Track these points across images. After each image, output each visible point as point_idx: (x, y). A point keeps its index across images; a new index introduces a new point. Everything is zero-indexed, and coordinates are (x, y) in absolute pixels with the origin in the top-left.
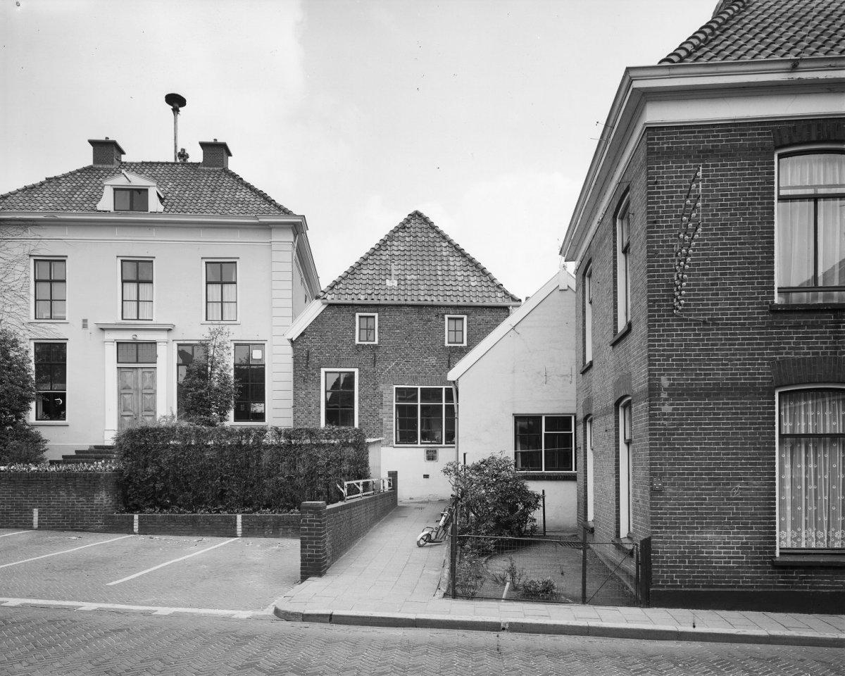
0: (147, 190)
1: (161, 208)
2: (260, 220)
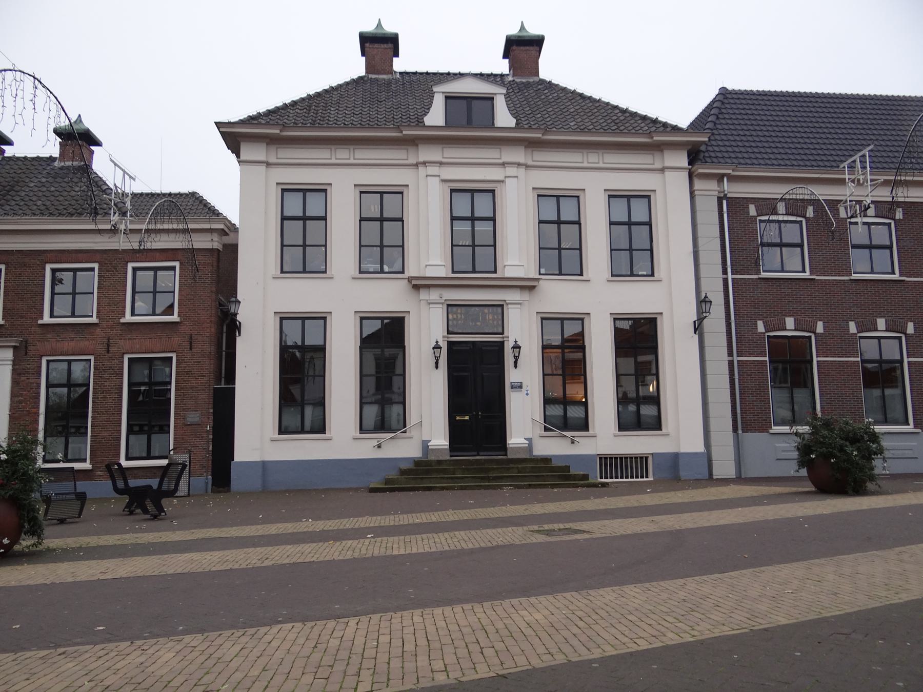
0: (492, 99)
1: (511, 122)
2: (655, 138)
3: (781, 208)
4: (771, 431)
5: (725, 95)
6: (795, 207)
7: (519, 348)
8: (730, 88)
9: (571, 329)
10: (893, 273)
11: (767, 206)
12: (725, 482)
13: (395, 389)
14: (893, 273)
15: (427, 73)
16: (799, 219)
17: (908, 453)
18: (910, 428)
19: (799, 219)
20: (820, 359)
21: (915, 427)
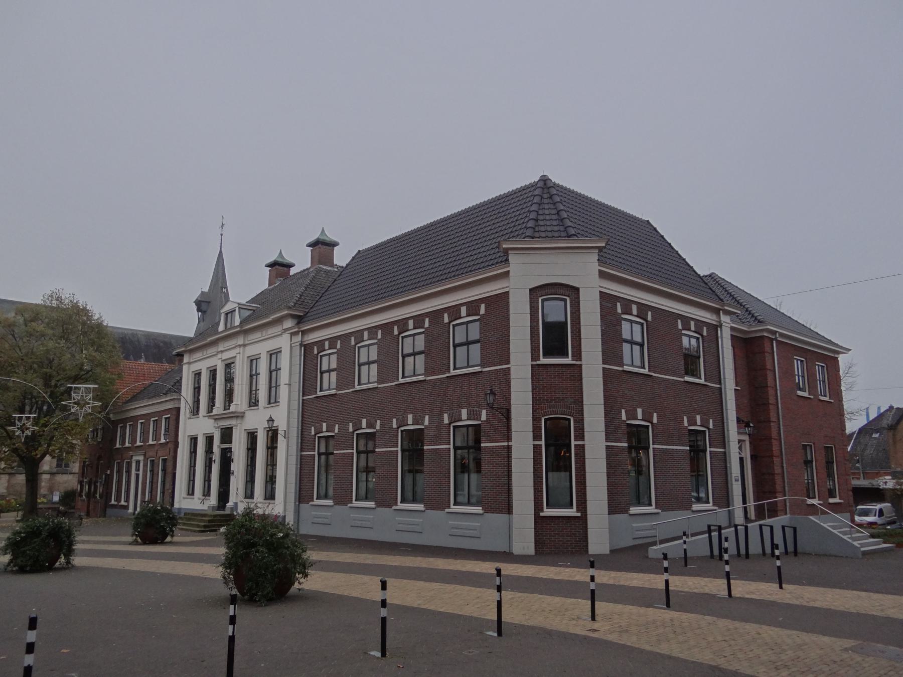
6: (643, 309)
8: (556, 179)
11: (627, 304)
13: (779, 488)
18: (651, 509)
21: (714, 505)
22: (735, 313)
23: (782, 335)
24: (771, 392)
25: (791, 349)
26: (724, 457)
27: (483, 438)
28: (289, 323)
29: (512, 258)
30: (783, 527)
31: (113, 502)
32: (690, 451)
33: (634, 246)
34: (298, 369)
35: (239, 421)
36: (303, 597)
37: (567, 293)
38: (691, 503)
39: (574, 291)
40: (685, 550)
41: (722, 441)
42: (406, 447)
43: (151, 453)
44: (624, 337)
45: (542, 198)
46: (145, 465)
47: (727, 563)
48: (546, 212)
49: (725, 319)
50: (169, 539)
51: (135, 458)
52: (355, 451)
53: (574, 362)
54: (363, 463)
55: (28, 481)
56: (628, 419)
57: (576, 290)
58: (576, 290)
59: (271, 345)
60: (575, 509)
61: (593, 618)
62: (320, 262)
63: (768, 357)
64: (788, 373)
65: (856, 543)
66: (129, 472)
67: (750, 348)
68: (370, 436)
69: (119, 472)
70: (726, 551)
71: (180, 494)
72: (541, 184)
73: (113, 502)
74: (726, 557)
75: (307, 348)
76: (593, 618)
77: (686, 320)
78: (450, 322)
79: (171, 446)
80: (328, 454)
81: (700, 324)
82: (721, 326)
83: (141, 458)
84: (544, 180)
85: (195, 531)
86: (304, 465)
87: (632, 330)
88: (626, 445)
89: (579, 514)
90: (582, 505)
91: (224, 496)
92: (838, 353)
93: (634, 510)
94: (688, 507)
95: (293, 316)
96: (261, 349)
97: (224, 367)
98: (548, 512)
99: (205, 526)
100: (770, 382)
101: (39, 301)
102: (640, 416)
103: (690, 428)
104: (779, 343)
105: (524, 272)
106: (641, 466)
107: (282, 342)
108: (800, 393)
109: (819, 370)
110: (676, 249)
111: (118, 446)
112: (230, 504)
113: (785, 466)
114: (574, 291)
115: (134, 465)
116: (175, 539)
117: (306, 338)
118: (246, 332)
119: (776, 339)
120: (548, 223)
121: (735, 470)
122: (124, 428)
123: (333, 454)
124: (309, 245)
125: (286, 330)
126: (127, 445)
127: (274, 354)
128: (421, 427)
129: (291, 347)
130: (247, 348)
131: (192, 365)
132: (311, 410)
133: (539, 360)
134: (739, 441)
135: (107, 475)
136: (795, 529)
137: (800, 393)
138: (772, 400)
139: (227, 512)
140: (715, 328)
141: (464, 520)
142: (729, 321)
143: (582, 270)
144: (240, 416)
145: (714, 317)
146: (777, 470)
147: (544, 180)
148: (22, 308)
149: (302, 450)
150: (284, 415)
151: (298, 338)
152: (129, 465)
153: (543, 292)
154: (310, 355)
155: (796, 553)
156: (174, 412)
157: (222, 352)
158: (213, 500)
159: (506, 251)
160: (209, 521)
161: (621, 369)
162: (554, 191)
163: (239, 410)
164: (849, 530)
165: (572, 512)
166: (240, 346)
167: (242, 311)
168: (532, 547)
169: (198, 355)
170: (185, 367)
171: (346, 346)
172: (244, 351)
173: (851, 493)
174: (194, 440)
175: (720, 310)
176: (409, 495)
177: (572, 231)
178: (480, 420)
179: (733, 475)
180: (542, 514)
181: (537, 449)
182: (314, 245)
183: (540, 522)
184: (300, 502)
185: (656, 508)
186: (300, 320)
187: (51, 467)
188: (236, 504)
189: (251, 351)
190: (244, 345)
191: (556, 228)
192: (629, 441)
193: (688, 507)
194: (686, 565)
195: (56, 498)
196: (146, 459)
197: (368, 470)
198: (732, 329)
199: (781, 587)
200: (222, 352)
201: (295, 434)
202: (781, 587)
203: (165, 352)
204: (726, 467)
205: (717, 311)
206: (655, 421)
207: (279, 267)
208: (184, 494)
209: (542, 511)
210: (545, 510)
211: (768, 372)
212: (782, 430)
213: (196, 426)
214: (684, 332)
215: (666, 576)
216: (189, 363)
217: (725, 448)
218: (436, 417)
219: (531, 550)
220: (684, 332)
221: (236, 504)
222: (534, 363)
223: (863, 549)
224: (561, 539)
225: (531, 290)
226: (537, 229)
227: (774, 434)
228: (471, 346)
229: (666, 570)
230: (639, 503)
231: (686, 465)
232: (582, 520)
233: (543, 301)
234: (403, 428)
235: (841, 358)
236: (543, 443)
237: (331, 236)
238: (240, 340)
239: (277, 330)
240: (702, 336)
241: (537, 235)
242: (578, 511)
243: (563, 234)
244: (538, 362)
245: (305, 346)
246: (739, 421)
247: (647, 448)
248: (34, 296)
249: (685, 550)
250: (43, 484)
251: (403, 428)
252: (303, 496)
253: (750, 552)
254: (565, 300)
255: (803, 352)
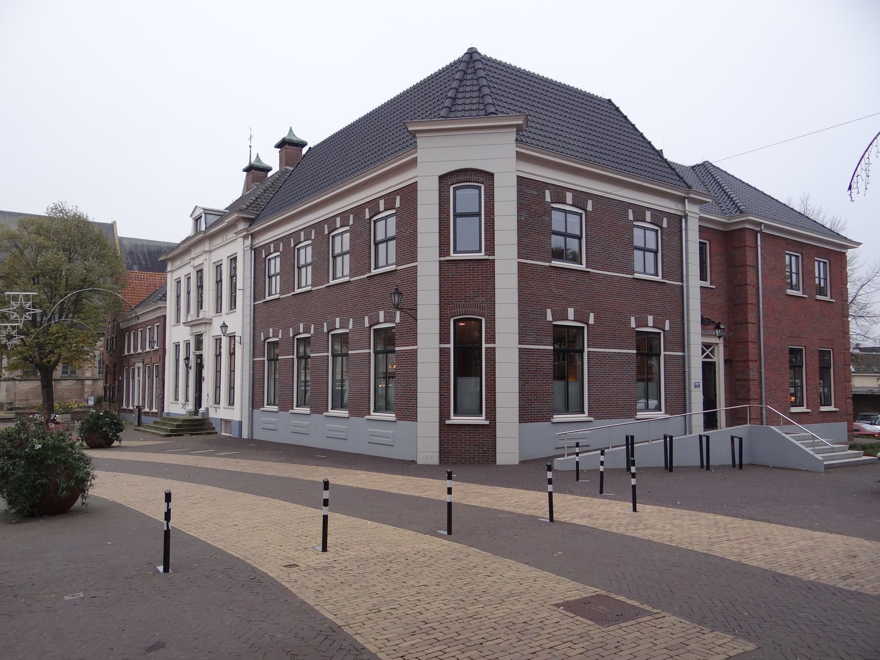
3: (569, 197)
4: (554, 420)
5: (472, 58)
6: (580, 198)
7: (791, 367)
8: (483, 51)
9: (199, 268)
10: (657, 275)
11: (559, 193)
12: (687, 469)
13: (753, 395)
14: (657, 275)
15: (617, 109)
16: (656, 228)
17: (304, 430)
18: (584, 417)
19: (656, 228)
20: (591, 349)
21: (589, 416)
22: (707, 202)
23: (767, 226)
24: (751, 290)
25: (780, 243)
26: (683, 362)
27: (397, 342)
28: (242, 226)
29: (421, 141)
30: (732, 438)
31: (124, 407)
32: (637, 354)
33: (589, 127)
34: (250, 274)
35: (208, 327)
36: (72, 511)
37: (481, 179)
38: (636, 411)
39: (488, 177)
40: (577, 462)
41: (680, 341)
42: (577, 356)
43: (147, 361)
44: (554, 228)
45: (465, 73)
46: (144, 372)
47: (634, 476)
48: (472, 88)
49: (689, 207)
50: (116, 443)
51: (137, 365)
52: (295, 357)
53: (486, 257)
54: (382, 369)
55: (43, 387)
56: (637, 326)
57: (491, 175)
58: (491, 175)
59: (228, 251)
60: (484, 417)
61: (325, 549)
62: (287, 165)
63: (749, 253)
64: (776, 269)
65: (819, 457)
66: (133, 378)
67: (729, 245)
68: (306, 341)
69: (128, 379)
70: (633, 464)
71: (168, 398)
72: (467, 58)
73: (124, 407)
74: (633, 469)
75: (256, 251)
76: (325, 549)
77: (640, 212)
78: (371, 218)
79: (160, 353)
80: (306, 357)
81: (658, 216)
82: (686, 216)
83: (141, 365)
84: (472, 53)
85: (161, 435)
86: (256, 370)
87: (566, 220)
88: (635, 352)
89: (487, 422)
90: (492, 414)
91: (198, 402)
92: (847, 247)
93: (557, 418)
94: (548, 419)
95: (245, 219)
96: (222, 255)
97: (195, 273)
98: (455, 420)
99: (172, 431)
100: (750, 278)
101: (42, 212)
102: (651, 323)
103: (555, 323)
104: (763, 234)
105: (436, 156)
106: (652, 374)
107: (237, 246)
108: (790, 292)
109: (819, 269)
110: (641, 131)
111: (126, 353)
112: (202, 410)
113: (766, 371)
114: (488, 177)
115: (136, 371)
116: (124, 443)
117: (257, 241)
118: (212, 237)
119: (761, 232)
120: (467, 101)
121: (696, 374)
122: (136, 335)
123: (309, 357)
124: (277, 146)
125: (237, 233)
126: (132, 352)
127: (233, 260)
128: (347, 331)
129: (244, 251)
130: (213, 254)
131: (175, 273)
132: (263, 315)
133: (449, 255)
134: (706, 346)
135: (119, 381)
136: (741, 439)
137: (790, 292)
138: (751, 299)
139: (199, 417)
140: (678, 220)
141: (377, 429)
142: (697, 211)
143: (498, 154)
144: (208, 323)
145: (680, 207)
146: (753, 374)
147: (472, 53)
148: (27, 221)
149: (254, 356)
150: (238, 321)
151: (248, 242)
152: (134, 370)
153: (455, 180)
154: (259, 256)
155: (708, 468)
156: (162, 320)
157: (194, 259)
158: (191, 407)
159: (413, 134)
160: (178, 426)
161: (547, 264)
162: (479, 65)
163: (207, 317)
164: (818, 443)
165: (481, 420)
166: (206, 252)
167: (208, 216)
168: (436, 455)
169: (178, 263)
170: (169, 275)
171: (288, 248)
172: (210, 259)
173: (850, 401)
174: (177, 346)
175: (685, 198)
176: (382, 403)
177: (492, 109)
178: (394, 322)
179: (693, 382)
180: (447, 422)
181: (443, 353)
182: (281, 145)
183: (445, 429)
184: (253, 408)
185: (589, 416)
186: (251, 222)
187: (93, 374)
188: (207, 409)
189: (217, 256)
190: (210, 252)
191: (474, 107)
192: (638, 348)
193: (631, 413)
194: (578, 479)
195: (91, 403)
196: (145, 366)
197: (388, 377)
198: (701, 219)
199: (635, 510)
200: (194, 259)
201: (248, 340)
202: (635, 510)
203: (154, 258)
204: (684, 372)
205: (682, 200)
206: (667, 328)
207: (255, 171)
208: (172, 399)
209: (449, 418)
210: (452, 417)
211: (748, 269)
212: (765, 335)
213: (178, 334)
214: (635, 223)
215: (325, 511)
216: (172, 271)
217: (684, 351)
218: (359, 321)
219: (435, 460)
220: (635, 223)
221: (207, 409)
222: (443, 259)
223: (825, 463)
224: (467, 451)
225: (442, 178)
226: (453, 109)
227: (752, 336)
228: (390, 243)
229: (326, 503)
230: (567, 410)
231: (631, 371)
232: (491, 429)
233: (455, 189)
234: (333, 333)
235: (850, 253)
236: (451, 346)
237: (283, 134)
238: (206, 247)
239: (231, 235)
240: (661, 227)
241: (452, 115)
242: (487, 419)
243: (482, 113)
244: (447, 258)
245: (255, 250)
246: (705, 322)
247: (659, 355)
248: (39, 207)
249: (577, 462)
250: (86, 390)
251: (333, 333)
252: (255, 402)
253: (711, 463)
254: (479, 188)
255: (799, 247)
